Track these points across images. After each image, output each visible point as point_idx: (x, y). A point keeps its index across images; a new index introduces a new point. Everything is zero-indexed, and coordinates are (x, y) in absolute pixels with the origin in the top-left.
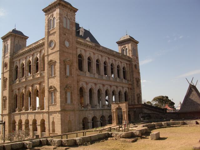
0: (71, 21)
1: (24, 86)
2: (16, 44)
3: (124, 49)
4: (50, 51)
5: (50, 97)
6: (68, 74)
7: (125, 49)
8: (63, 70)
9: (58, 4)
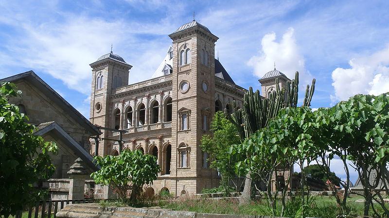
0: (209, 54)
1: (133, 139)
2: (115, 76)
3: (183, 49)
4: (181, 96)
5: (180, 158)
6: (205, 129)
7: (185, 50)
8: (200, 122)
9: (196, 31)
